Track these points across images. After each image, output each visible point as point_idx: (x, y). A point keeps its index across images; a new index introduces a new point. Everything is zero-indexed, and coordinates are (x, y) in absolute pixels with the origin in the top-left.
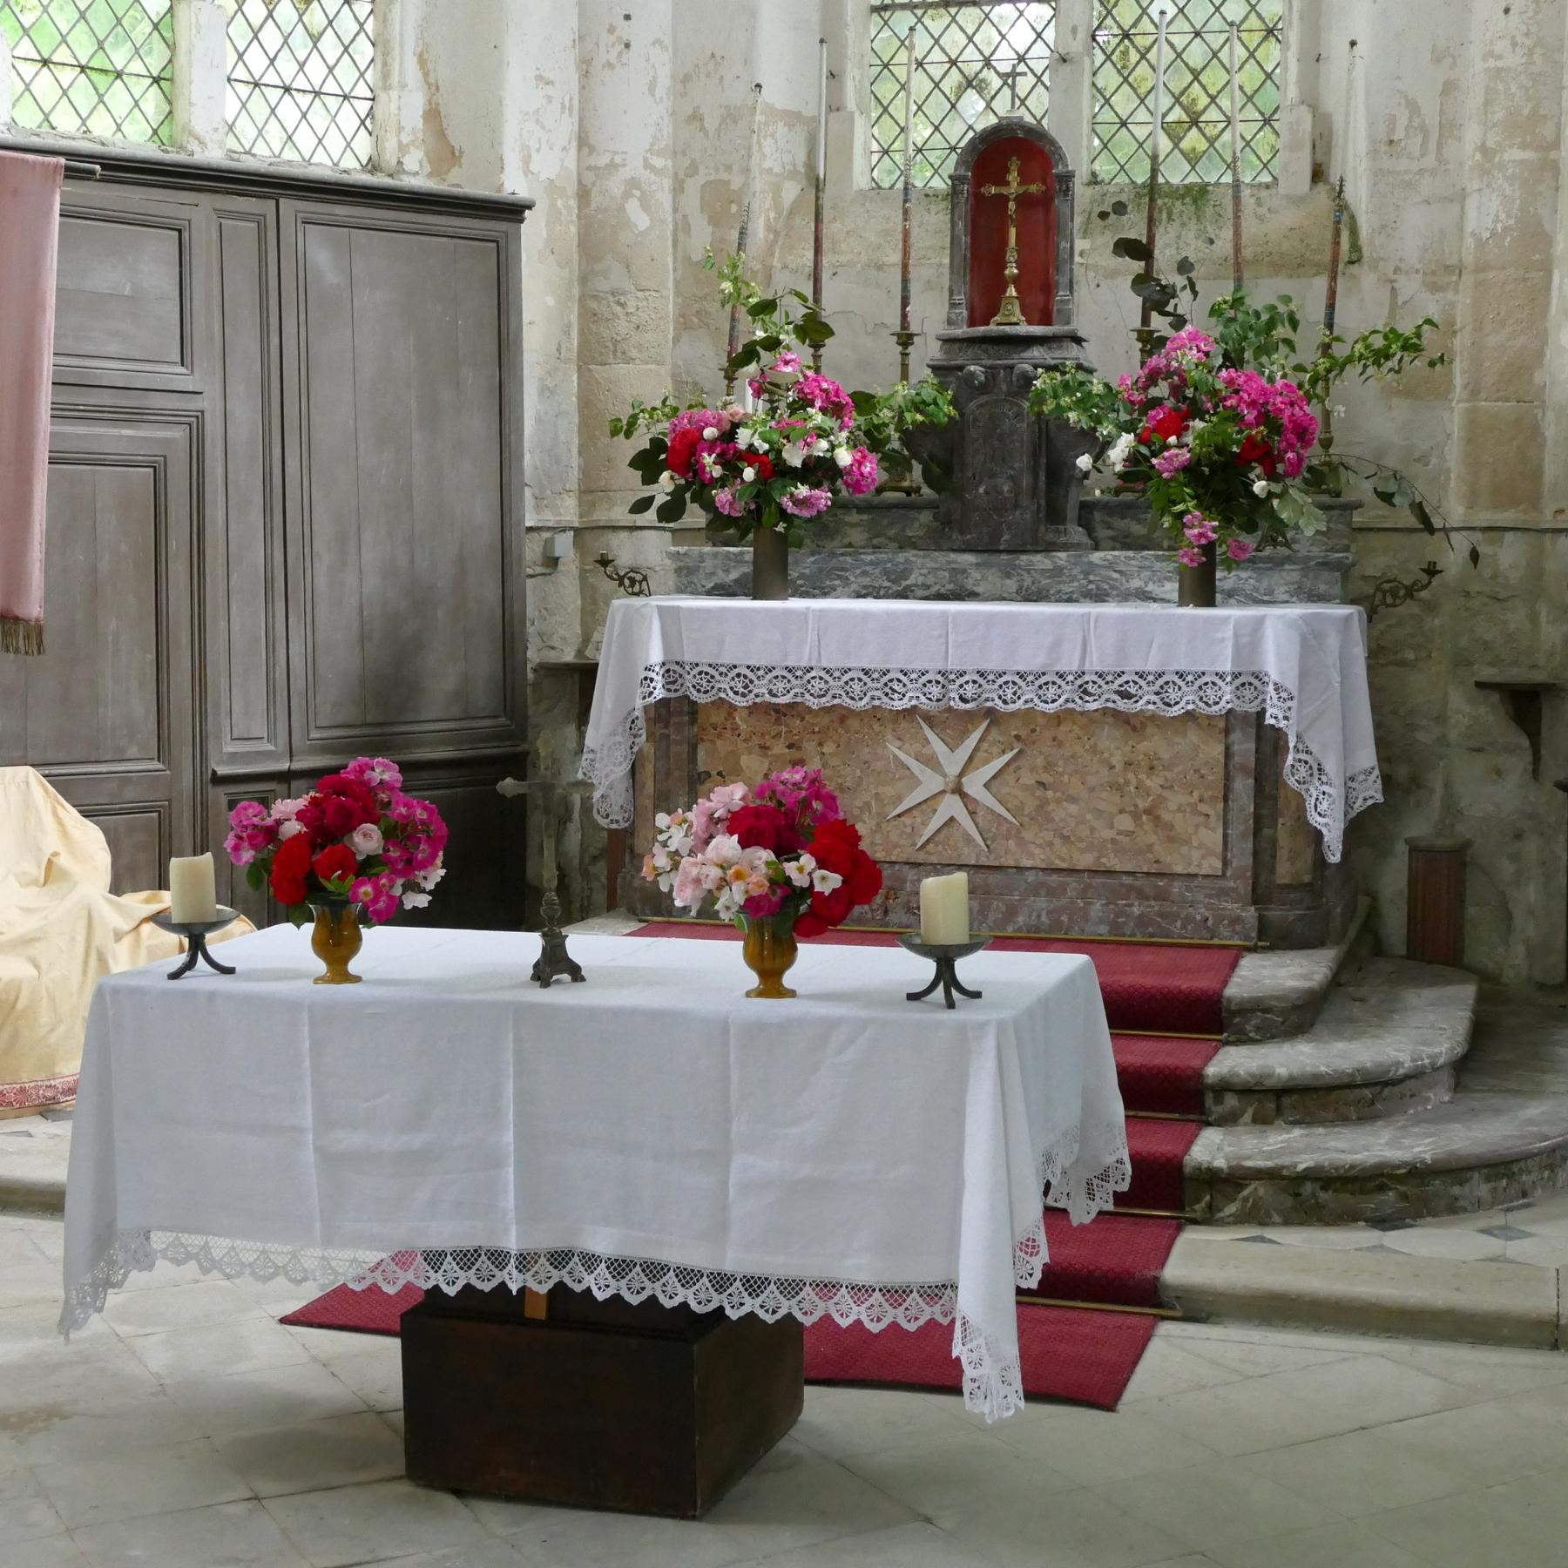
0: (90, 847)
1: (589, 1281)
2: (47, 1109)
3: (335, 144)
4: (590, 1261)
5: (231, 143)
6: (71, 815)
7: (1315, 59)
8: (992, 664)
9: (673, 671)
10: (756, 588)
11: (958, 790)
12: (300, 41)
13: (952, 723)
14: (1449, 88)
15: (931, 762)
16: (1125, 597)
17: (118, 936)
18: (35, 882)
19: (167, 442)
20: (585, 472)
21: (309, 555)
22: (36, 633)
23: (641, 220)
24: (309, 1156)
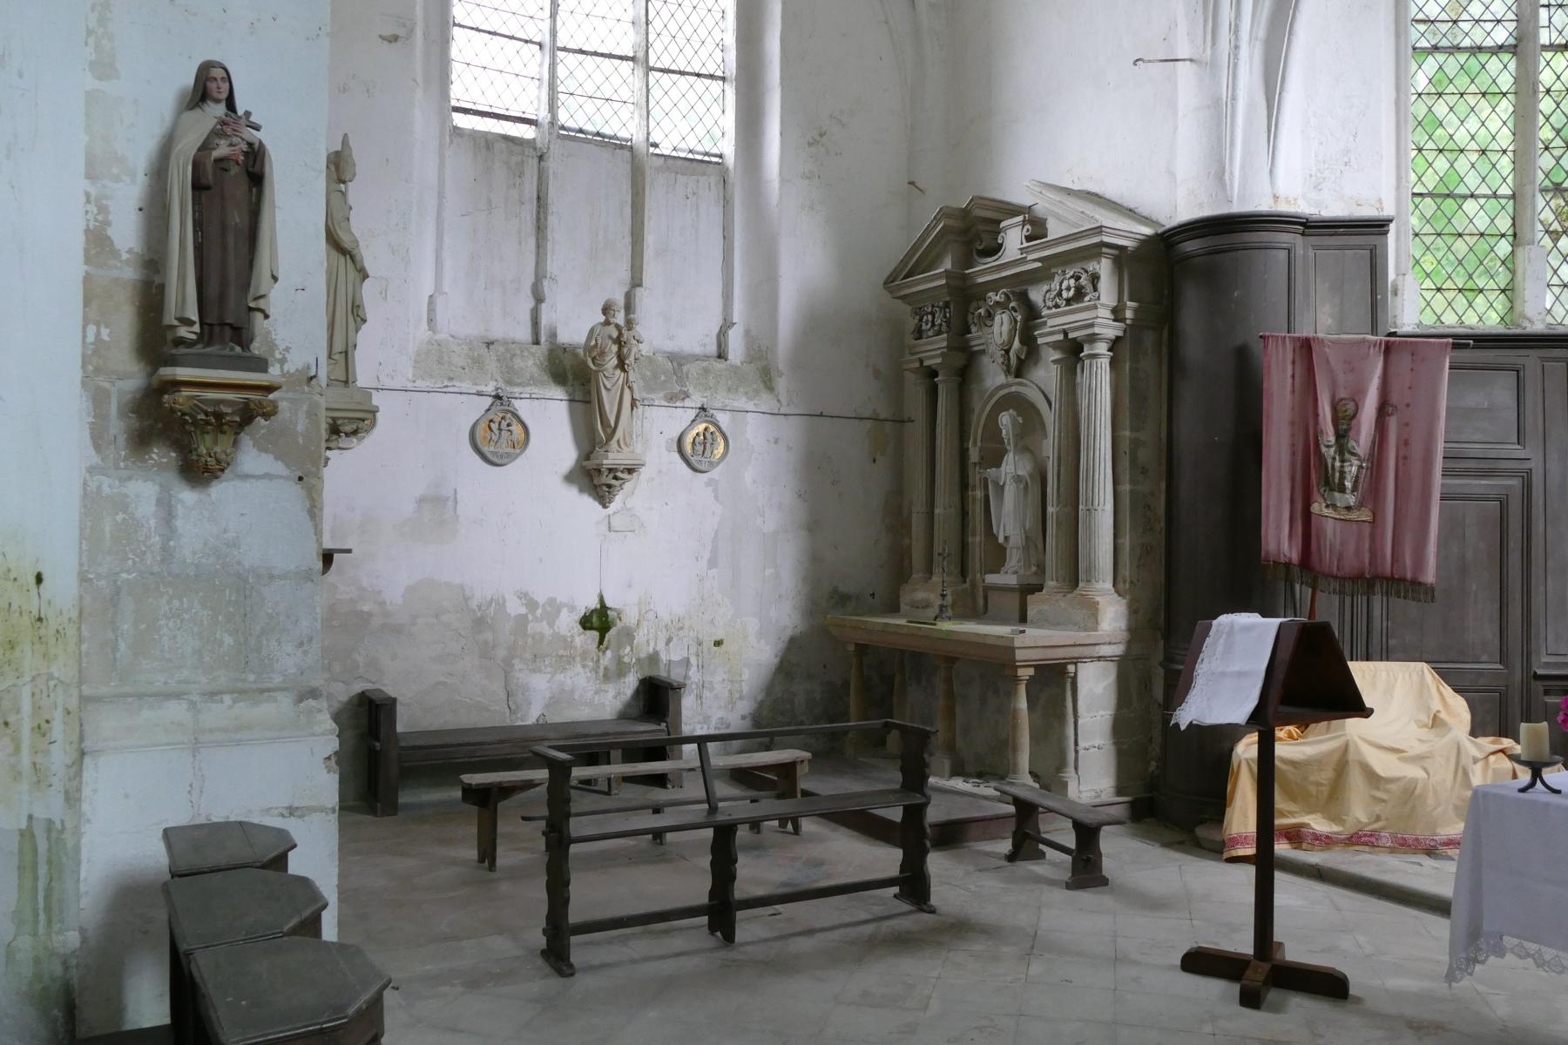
0: (1458, 710)
5: (1549, 319)
6: (1448, 691)
17: (1475, 761)
18: (1426, 726)
19: (1510, 486)
22: (1428, 592)
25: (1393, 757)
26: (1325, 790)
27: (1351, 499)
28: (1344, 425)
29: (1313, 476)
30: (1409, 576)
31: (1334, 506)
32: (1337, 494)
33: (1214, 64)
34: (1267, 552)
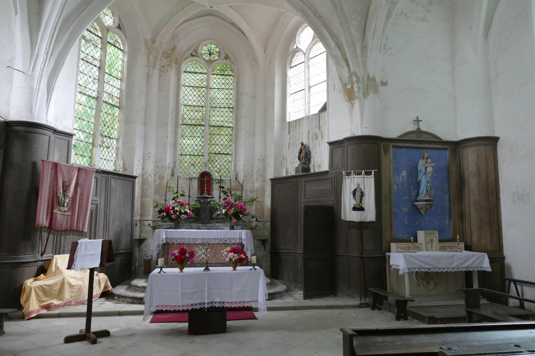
1: (215, 305)
2: (83, 304)
3: (110, 167)
4: (216, 303)
7: (235, 166)
8: (209, 237)
9: (166, 239)
10: (175, 228)
11: (204, 253)
12: (107, 153)
13: (203, 245)
14: (252, 170)
15: (201, 250)
16: (220, 229)
20: (141, 212)
21: (109, 225)
23: (150, 179)
24: (180, 293)
25: (74, 279)
26: (57, 292)
27: (66, 209)
28: (66, 189)
29: (55, 202)
30: (81, 230)
31: (60, 211)
32: (62, 207)
33: (32, 77)
34: (39, 224)
